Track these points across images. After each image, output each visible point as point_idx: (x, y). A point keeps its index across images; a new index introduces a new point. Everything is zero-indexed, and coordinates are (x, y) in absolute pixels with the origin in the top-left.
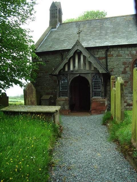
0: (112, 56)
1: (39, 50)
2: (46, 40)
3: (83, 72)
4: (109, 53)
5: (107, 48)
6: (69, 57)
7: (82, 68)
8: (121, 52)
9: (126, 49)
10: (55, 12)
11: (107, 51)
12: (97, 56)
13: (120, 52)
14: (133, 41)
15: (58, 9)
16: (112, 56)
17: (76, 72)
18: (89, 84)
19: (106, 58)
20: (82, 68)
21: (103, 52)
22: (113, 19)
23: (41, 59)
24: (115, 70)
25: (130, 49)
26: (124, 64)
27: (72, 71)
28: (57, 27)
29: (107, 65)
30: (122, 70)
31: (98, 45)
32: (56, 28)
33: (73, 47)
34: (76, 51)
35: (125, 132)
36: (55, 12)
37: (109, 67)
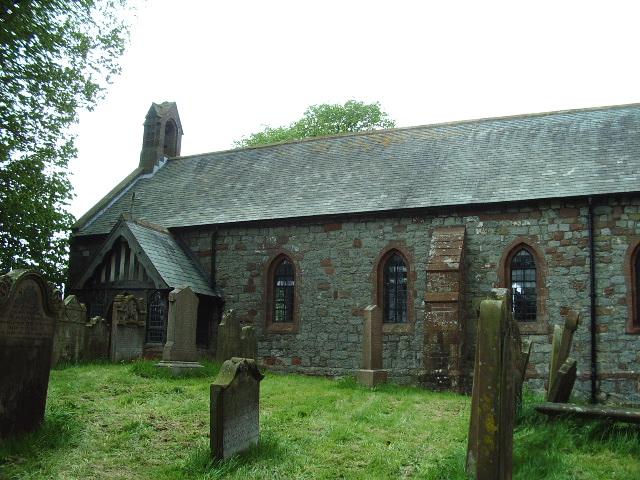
0: (226, 248)
1: (84, 232)
2: (116, 203)
3: (132, 287)
4: (218, 242)
5: (216, 230)
6: (104, 252)
7: (131, 276)
8: (246, 238)
9: (255, 232)
10: (162, 129)
11: (215, 237)
12: (195, 249)
13: (244, 238)
14: (626, 184)
15: (164, 123)
16: (226, 248)
17: (120, 284)
18: (221, 313)
19: (213, 254)
20: (131, 276)
21: (209, 240)
22: (578, 117)
23: (88, 252)
24: (231, 283)
25: (264, 232)
26: (251, 267)
27: (113, 283)
28: (156, 169)
29: (214, 271)
30: (245, 282)
31: (299, 214)
32: (151, 172)
33: (113, 231)
34: (116, 240)
35: (532, 432)
36: (162, 129)
37: (218, 276)
